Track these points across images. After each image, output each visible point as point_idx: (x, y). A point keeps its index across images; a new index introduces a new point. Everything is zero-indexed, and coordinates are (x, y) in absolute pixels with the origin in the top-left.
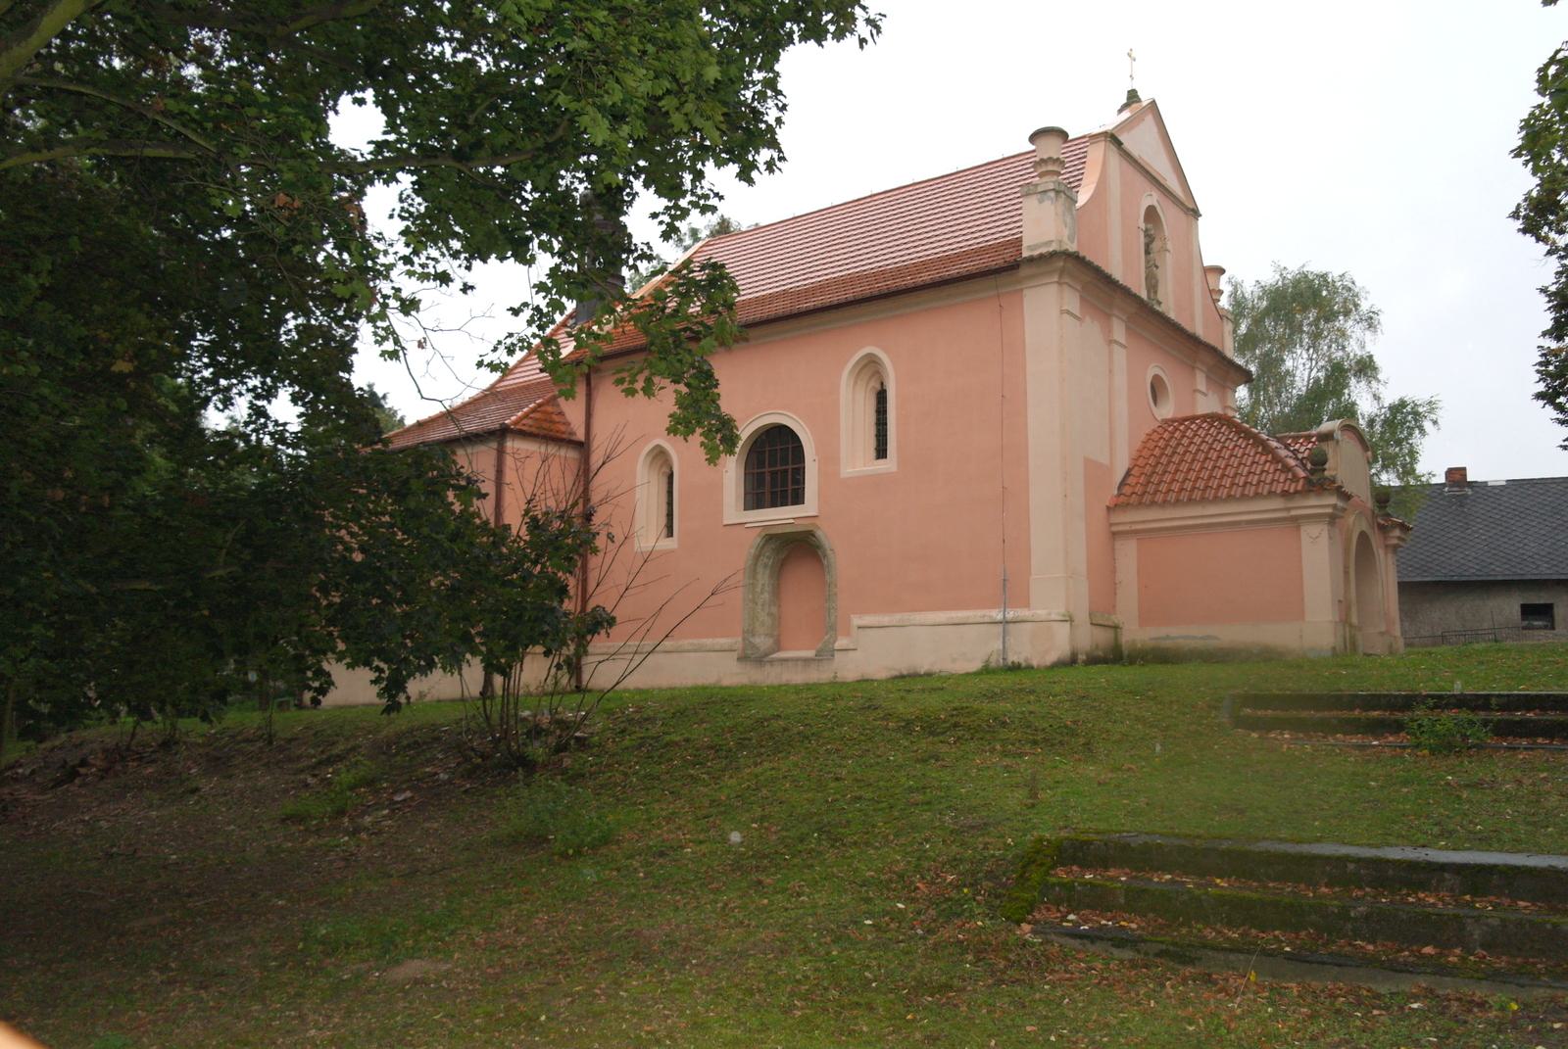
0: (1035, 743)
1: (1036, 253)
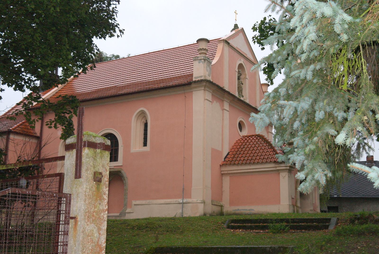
0: (168, 231)
1: (197, 79)
